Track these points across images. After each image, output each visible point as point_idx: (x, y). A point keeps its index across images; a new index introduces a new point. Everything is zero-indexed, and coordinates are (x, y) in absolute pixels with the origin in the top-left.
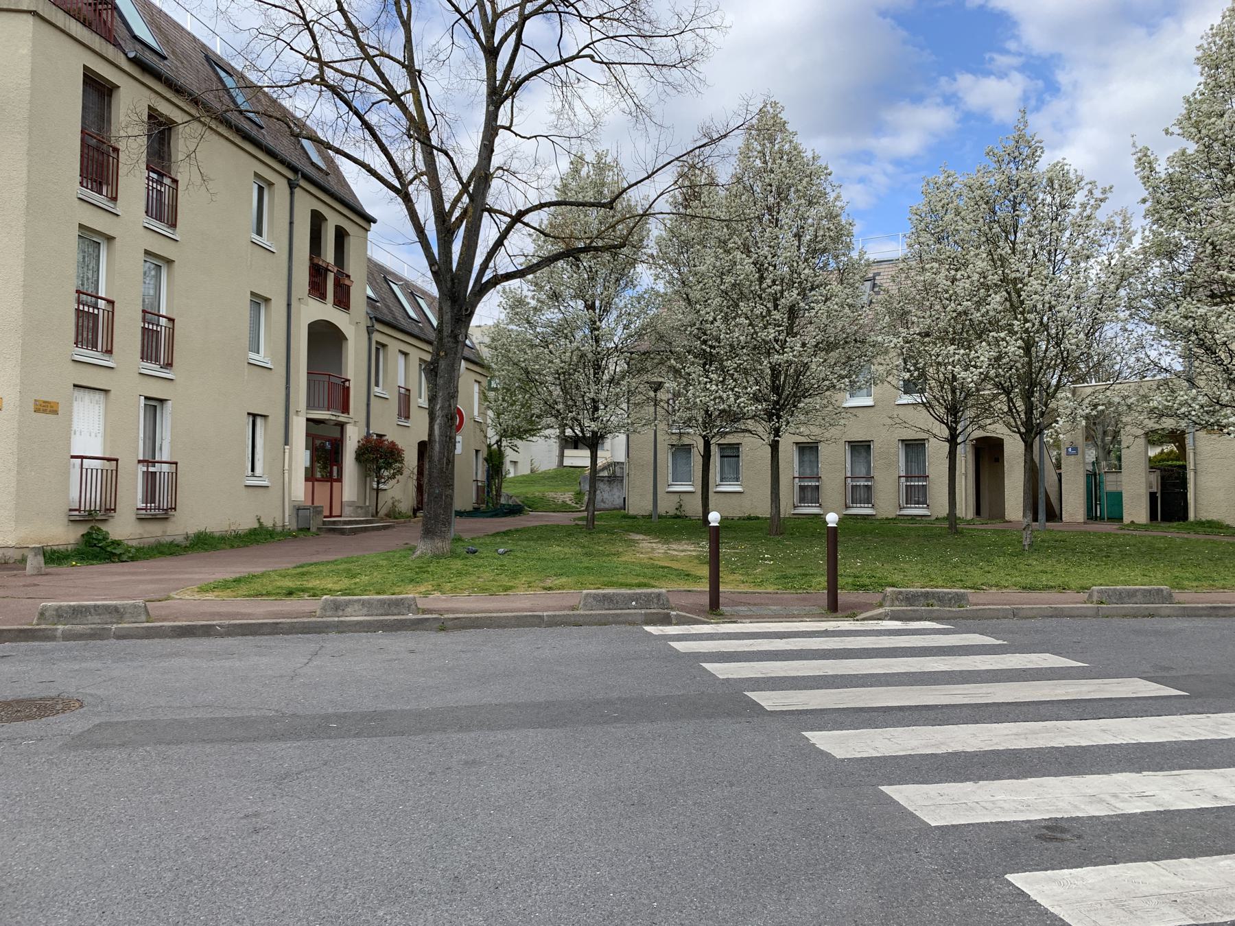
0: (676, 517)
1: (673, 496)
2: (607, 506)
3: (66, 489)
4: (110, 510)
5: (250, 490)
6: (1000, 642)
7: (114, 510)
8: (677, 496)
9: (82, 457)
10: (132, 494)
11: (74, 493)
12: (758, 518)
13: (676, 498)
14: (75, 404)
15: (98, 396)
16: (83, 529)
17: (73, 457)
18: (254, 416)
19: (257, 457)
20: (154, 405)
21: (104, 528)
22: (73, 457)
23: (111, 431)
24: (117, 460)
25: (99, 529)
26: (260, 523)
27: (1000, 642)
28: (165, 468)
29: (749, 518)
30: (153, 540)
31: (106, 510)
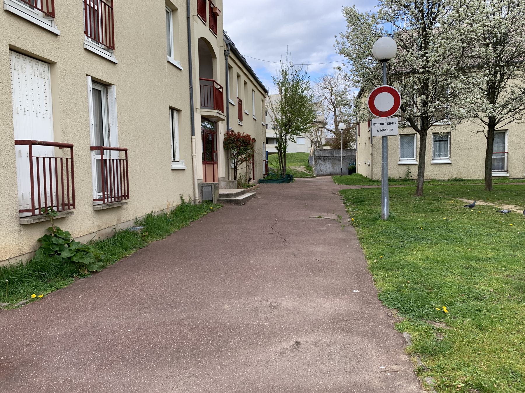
0: (405, 180)
1: (402, 167)
2: (323, 173)
3: (14, 185)
4: (69, 205)
5: (175, 173)
6: (243, 190)
7: (73, 205)
8: (407, 167)
9: (30, 143)
10: (88, 186)
11: (24, 188)
12: (461, 180)
13: (405, 169)
14: (14, 73)
15: (42, 68)
16: (38, 233)
17: (17, 142)
18: (172, 109)
19: (177, 144)
20: (101, 87)
21: (64, 227)
22: (17, 142)
23: (60, 111)
24: (71, 147)
25: (58, 229)
26: (183, 201)
27: (243, 190)
28: (115, 155)
29: (456, 180)
30: (109, 230)
31: (64, 205)
